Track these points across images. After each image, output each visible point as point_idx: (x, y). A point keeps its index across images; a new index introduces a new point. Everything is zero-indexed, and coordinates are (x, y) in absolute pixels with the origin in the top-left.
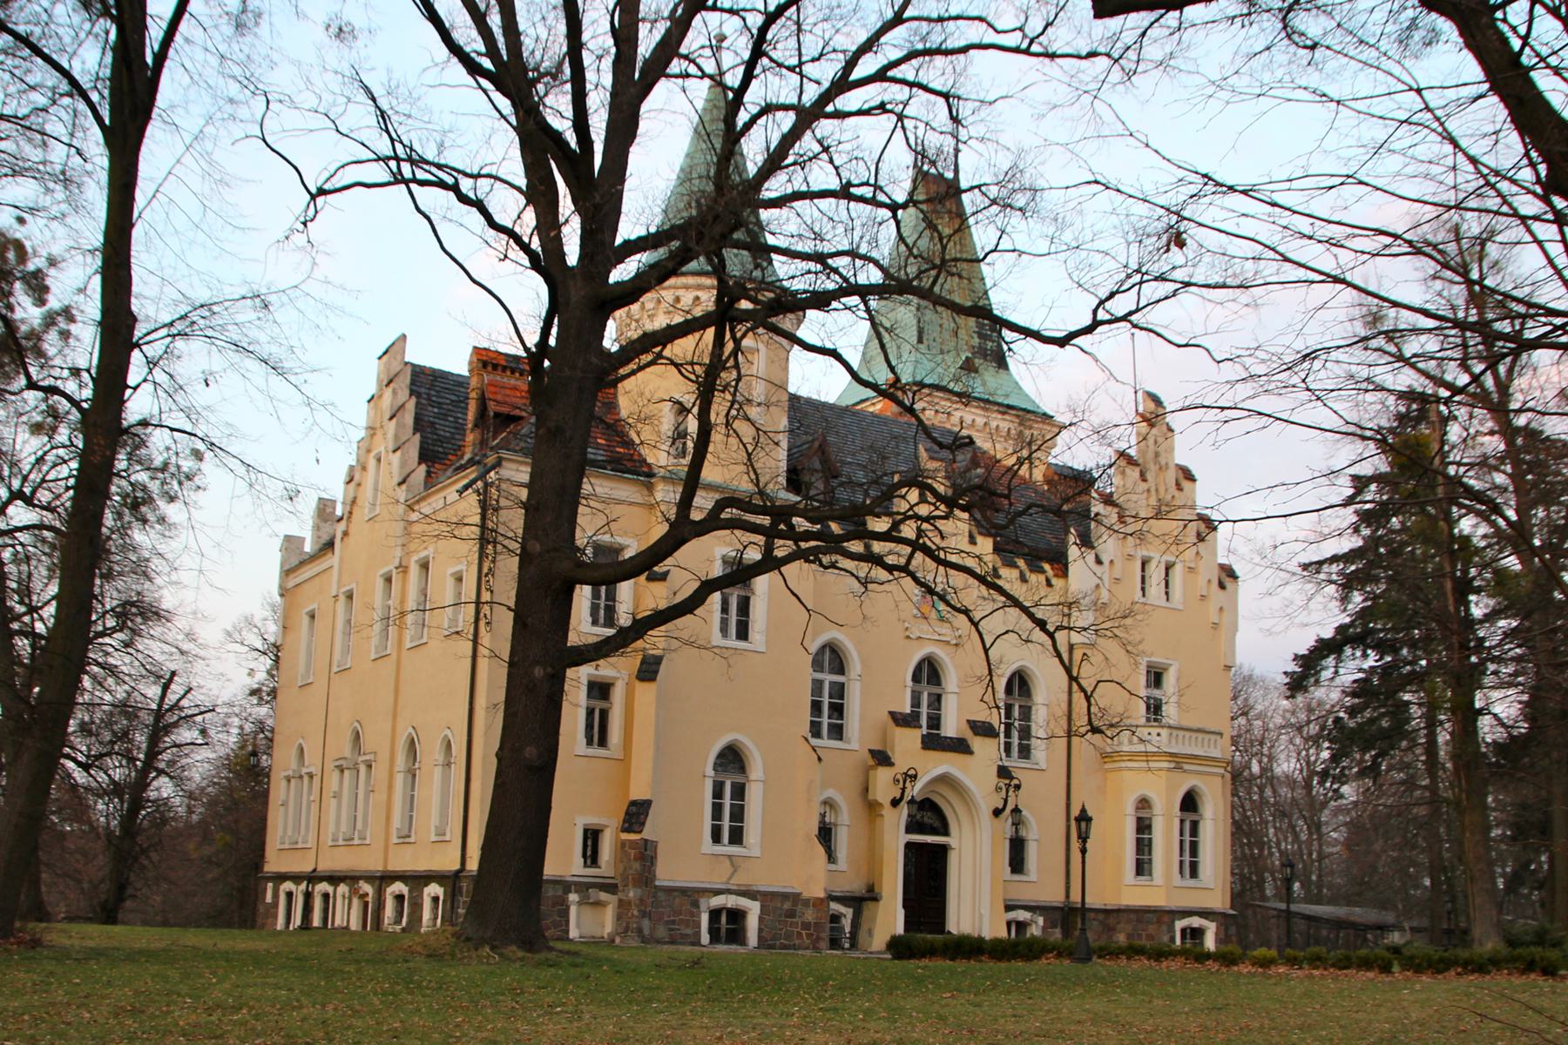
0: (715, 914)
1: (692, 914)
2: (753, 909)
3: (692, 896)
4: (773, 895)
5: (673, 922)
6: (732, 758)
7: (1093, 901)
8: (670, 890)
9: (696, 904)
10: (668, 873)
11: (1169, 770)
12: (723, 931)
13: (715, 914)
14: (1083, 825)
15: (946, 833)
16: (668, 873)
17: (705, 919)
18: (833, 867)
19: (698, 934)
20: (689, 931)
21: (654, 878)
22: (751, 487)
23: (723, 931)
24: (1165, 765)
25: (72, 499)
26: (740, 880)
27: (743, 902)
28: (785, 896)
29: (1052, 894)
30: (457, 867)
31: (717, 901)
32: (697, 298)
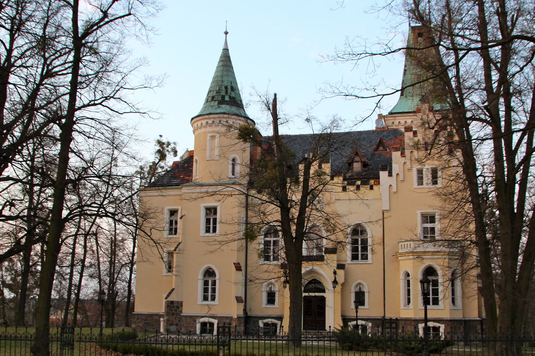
0: (204, 324)
1: (194, 324)
2: (215, 322)
3: (194, 318)
4: (223, 317)
5: (187, 327)
6: (209, 273)
7: (388, 316)
8: (186, 317)
9: (195, 321)
10: (186, 311)
11: (414, 259)
12: (208, 330)
13: (204, 324)
14: (426, 285)
15: (324, 291)
16: (186, 311)
17: (198, 326)
18: (455, 308)
19: (196, 330)
20: (193, 330)
21: (181, 312)
22: (214, 181)
23: (208, 330)
24: (411, 257)
25: (497, 197)
26: (211, 313)
27: (212, 320)
28: (227, 318)
29: (377, 314)
30: (383, 315)
31: (202, 320)
32: (207, 122)
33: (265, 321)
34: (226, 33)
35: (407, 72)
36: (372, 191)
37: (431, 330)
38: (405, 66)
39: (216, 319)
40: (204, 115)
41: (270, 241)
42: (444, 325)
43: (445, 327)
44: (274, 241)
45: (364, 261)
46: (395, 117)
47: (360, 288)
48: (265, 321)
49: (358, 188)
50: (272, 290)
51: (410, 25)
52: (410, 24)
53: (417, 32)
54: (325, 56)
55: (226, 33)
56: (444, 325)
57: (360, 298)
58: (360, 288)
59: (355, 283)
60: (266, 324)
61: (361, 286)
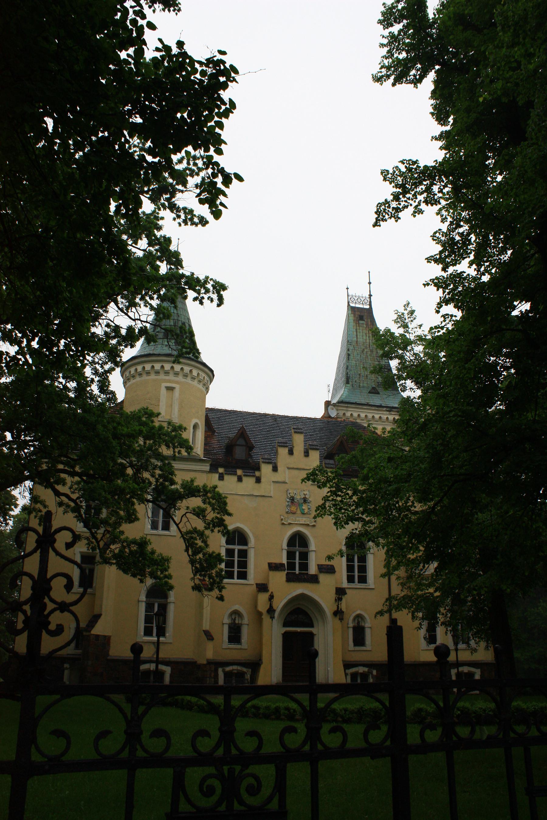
15: (312, 626)
33: (228, 669)
34: (347, 288)
35: (351, 357)
36: (240, 484)
37: (152, 678)
38: (348, 350)
39: (477, 668)
40: (159, 355)
41: (233, 550)
42: (479, 670)
43: (481, 672)
44: (239, 551)
45: (362, 585)
46: (347, 407)
47: (358, 622)
48: (228, 669)
49: (240, 479)
50: (237, 622)
51: (349, 305)
52: (348, 302)
53: (358, 313)
54: (205, 301)
55: (347, 288)
56: (479, 670)
57: (359, 638)
58: (358, 622)
59: (354, 615)
60: (458, 674)
61: (360, 620)
